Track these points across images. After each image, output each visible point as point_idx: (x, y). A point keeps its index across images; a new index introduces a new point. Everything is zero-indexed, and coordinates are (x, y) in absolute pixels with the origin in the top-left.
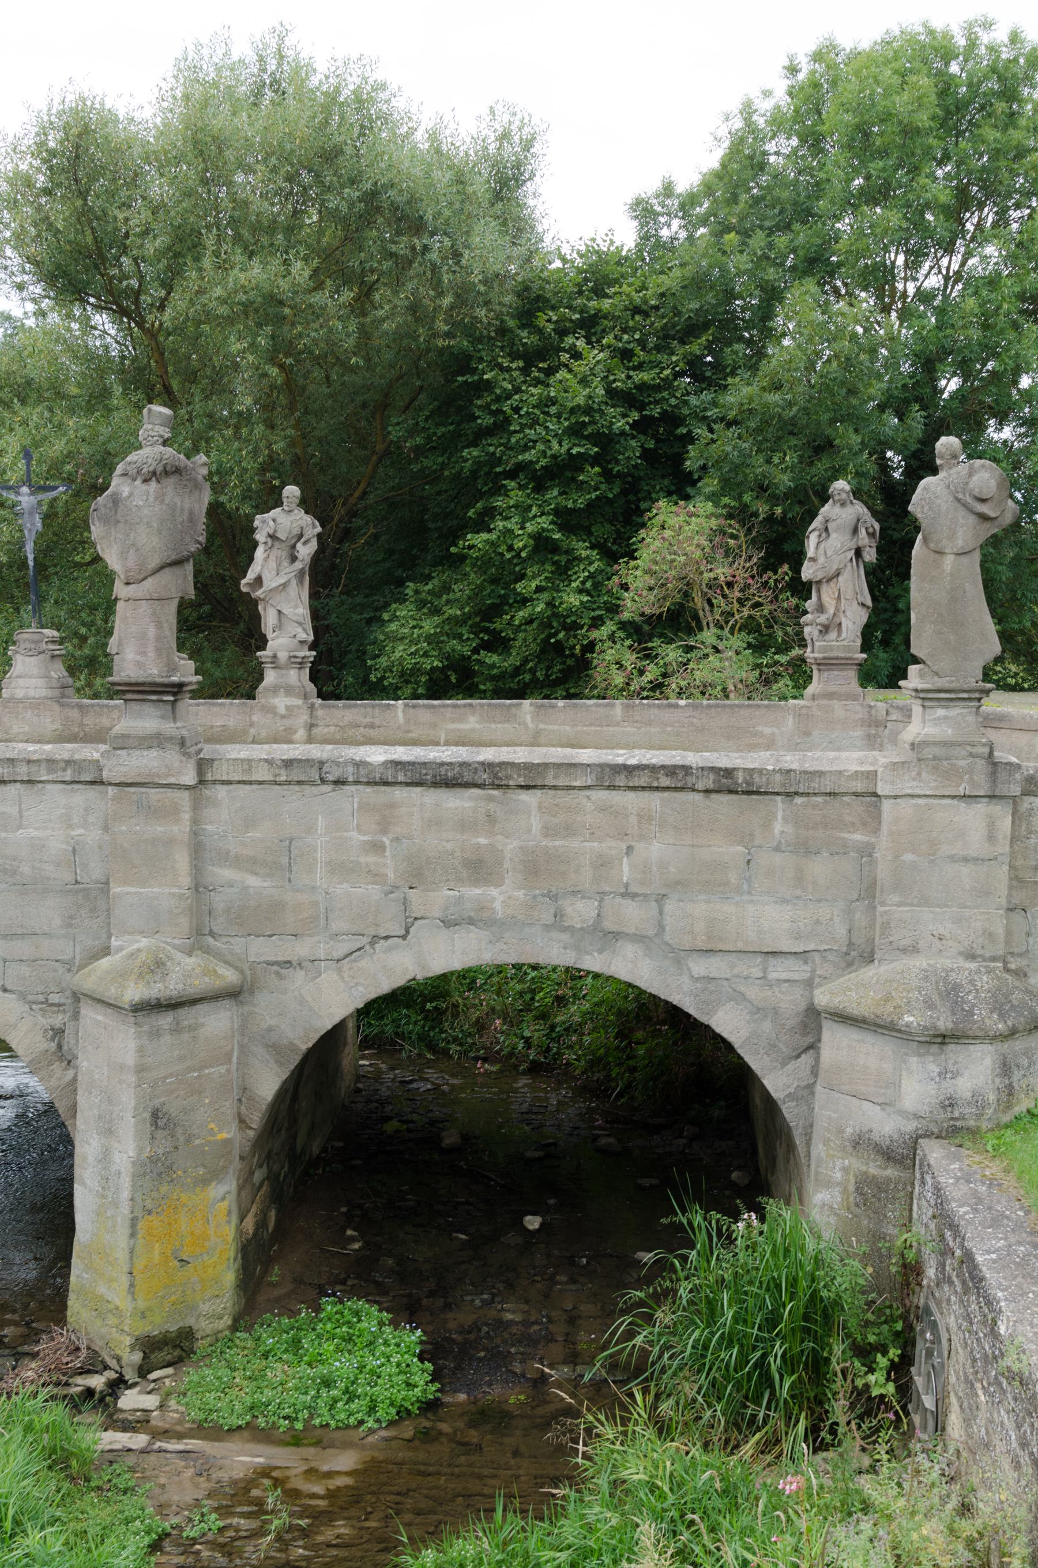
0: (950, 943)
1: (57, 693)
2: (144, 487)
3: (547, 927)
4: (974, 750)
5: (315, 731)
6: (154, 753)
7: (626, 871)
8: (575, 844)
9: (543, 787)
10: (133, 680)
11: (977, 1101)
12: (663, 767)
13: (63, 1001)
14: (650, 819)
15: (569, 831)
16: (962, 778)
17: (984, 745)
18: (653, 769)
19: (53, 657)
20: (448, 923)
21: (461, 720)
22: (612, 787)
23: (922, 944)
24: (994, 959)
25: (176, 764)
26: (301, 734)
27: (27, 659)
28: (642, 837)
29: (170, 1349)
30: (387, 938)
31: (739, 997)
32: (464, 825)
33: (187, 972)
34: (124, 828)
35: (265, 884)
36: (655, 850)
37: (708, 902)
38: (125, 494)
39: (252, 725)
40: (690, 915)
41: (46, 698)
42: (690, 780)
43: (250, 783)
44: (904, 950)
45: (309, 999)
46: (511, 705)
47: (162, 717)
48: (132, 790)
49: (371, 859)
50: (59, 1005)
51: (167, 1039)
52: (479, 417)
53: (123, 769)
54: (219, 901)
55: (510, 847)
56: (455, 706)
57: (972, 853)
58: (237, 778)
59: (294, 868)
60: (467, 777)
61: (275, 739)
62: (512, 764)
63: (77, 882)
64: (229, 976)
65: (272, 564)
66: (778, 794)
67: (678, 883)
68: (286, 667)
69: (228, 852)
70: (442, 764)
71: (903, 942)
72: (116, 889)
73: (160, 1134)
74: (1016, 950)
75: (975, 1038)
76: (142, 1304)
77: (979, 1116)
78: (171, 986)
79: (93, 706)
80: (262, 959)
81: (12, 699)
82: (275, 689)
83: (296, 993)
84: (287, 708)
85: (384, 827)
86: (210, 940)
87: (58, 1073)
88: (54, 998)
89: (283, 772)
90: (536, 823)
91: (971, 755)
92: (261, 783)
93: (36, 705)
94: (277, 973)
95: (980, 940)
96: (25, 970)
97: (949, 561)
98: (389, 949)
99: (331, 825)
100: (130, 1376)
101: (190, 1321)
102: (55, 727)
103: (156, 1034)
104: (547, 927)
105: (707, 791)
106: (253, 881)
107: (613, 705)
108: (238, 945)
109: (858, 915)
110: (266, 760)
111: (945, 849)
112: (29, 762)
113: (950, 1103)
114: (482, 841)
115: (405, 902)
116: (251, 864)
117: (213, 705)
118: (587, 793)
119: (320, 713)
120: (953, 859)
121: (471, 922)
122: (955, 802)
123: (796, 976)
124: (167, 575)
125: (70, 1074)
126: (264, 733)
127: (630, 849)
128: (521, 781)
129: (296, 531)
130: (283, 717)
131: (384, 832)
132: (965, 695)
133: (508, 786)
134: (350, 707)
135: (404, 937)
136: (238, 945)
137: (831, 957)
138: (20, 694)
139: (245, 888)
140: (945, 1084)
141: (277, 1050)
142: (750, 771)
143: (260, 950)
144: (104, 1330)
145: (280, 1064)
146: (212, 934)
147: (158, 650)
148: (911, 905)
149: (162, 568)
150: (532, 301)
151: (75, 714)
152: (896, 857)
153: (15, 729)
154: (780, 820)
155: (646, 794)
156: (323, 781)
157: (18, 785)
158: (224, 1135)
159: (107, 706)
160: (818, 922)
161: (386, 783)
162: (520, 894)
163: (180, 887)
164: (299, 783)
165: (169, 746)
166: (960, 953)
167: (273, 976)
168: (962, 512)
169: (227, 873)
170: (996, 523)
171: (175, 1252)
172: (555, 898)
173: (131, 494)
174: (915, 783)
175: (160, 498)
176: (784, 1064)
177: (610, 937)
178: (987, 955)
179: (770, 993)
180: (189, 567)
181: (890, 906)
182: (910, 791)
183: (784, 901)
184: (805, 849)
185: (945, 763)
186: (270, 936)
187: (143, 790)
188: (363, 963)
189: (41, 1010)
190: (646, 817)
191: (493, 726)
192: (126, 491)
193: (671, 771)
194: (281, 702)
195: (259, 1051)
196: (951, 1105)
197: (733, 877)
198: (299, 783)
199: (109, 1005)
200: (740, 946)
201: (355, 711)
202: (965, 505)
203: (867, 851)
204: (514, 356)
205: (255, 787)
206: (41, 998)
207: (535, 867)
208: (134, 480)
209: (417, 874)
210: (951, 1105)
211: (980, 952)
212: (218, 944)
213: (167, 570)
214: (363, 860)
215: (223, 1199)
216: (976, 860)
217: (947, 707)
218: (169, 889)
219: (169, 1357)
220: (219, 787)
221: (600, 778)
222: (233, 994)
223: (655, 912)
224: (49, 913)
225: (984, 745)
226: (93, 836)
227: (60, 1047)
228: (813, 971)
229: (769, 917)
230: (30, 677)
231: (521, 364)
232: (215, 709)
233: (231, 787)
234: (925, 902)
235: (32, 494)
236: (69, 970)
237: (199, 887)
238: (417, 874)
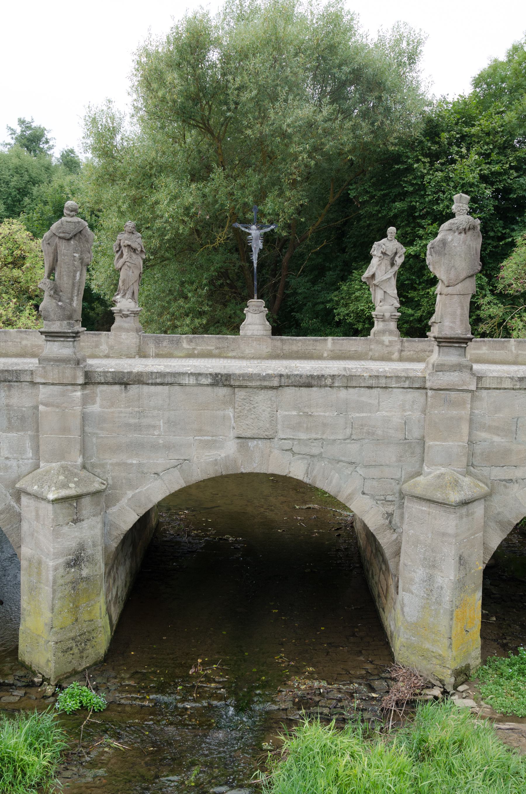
2: (459, 236)
5: (403, 353)
6: (456, 374)
10: (449, 336)
13: (393, 499)
21: (479, 348)
25: (468, 380)
26: (396, 355)
27: (254, 315)
34: (436, 412)
35: (503, 440)
38: (449, 240)
39: (371, 350)
41: (263, 335)
43: (500, 389)
45: (520, 498)
46: (504, 341)
47: (460, 355)
48: (442, 392)
50: (392, 501)
52: (405, 187)
53: (440, 382)
54: (478, 449)
58: (494, 387)
59: (518, 432)
61: (383, 359)
63: (405, 439)
65: (383, 267)
68: (388, 321)
69: (485, 424)
72: (429, 443)
79: (288, 340)
80: (498, 478)
81: (245, 336)
82: (121, 328)
83: (513, 495)
84: (390, 342)
86: (472, 468)
87: (388, 536)
88: (389, 498)
89: (518, 383)
92: (505, 389)
93: (258, 339)
94: (505, 485)
96: (375, 483)
102: (268, 350)
108: (486, 471)
110: (510, 378)
112: (386, 377)
116: (495, 430)
117: (351, 339)
119: (406, 344)
125: (395, 536)
126: (377, 355)
129: (394, 251)
130: (387, 346)
134: (422, 341)
136: (486, 471)
138: (249, 333)
139: (493, 442)
141: (501, 524)
143: (497, 473)
144: (429, 666)
145: (503, 531)
149: (464, 280)
150: (433, 129)
151: (279, 344)
153: (247, 351)
157: (379, 389)
159: (296, 340)
163: (463, 442)
165: (465, 370)
167: (502, 487)
169: (483, 435)
173: (452, 240)
180: (475, 278)
186: (503, 467)
187: (448, 392)
189: (382, 503)
191: (495, 352)
192: (450, 238)
194: (386, 339)
195: (492, 524)
199: (441, 503)
201: (424, 343)
204: (426, 156)
205: (502, 391)
206: (382, 498)
208: (455, 232)
212: (476, 471)
213: (468, 279)
218: (456, 444)
219: (462, 679)
220: (483, 391)
222: (486, 497)
224: (390, 455)
226: (416, 415)
227: (390, 522)
230: (255, 324)
231: (429, 160)
232: (351, 342)
233: (489, 391)
235: (258, 229)
236: (398, 484)
237: (471, 442)
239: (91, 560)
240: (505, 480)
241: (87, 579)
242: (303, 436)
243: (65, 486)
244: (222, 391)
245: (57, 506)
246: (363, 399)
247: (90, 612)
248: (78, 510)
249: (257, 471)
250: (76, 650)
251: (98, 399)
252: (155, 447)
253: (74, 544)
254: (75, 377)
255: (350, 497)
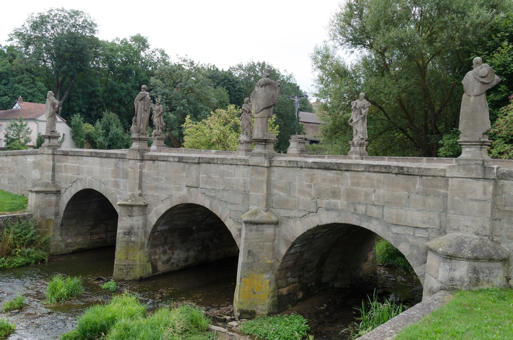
0: (470, 229)
1: (299, 152)
3: (352, 213)
4: (477, 162)
6: (259, 158)
7: (373, 198)
8: (360, 188)
9: (351, 171)
11: (461, 280)
12: (383, 166)
14: (380, 182)
15: (358, 184)
16: (473, 172)
17: (480, 160)
18: (380, 166)
19: (299, 143)
20: (327, 210)
22: (369, 171)
23: (461, 228)
24: (485, 236)
28: (378, 187)
29: (249, 315)
30: (312, 212)
31: (407, 241)
32: (331, 181)
33: (263, 216)
36: (381, 191)
37: (396, 209)
40: (391, 213)
42: (391, 170)
43: (281, 167)
44: (455, 230)
49: (308, 189)
51: (254, 232)
54: (274, 198)
55: (343, 188)
56: (403, 159)
57: (478, 198)
60: (332, 167)
62: (343, 164)
64: (274, 219)
66: (417, 175)
67: (388, 202)
68: (356, 146)
70: (325, 163)
71: (454, 227)
73: (250, 257)
74: (497, 234)
75: (461, 258)
76: (241, 301)
77: (462, 286)
78: (257, 219)
82: (352, 152)
85: (312, 180)
90: (349, 183)
91: (476, 164)
92: (284, 167)
95: (481, 229)
96: (234, 213)
97: (472, 98)
98: (312, 216)
99: (300, 179)
100: (237, 319)
101: (255, 309)
103: (251, 230)
104: (352, 213)
105: (396, 174)
106: (282, 194)
107: (452, 160)
109: (443, 217)
111: (469, 196)
112: (236, 159)
113: (452, 280)
114: (336, 186)
115: (316, 203)
116: (281, 189)
118: (363, 173)
120: (471, 200)
121: (333, 210)
122: (472, 180)
123: (424, 236)
124: (265, 111)
127: (374, 190)
128: (345, 169)
131: (312, 182)
132: (475, 143)
133: (342, 170)
135: (316, 213)
137: (435, 230)
138: (291, 152)
140: (451, 273)
141: (286, 241)
142: (408, 168)
143: (283, 213)
146: (273, 207)
147: (261, 131)
148: (458, 214)
149: (263, 109)
152: (452, 198)
154: (418, 184)
155: (379, 174)
156: (298, 167)
158: (269, 262)
160: (430, 218)
161: (312, 168)
162: (345, 202)
164: (292, 167)
166: (474, 233)
168: (476, 82)
170: (490, 85)
171: (252, 289)
172: (354, 204)
174: (458, 173)
175: (265, 91)
176: (420, 265)
177: (370, 218)
178: (483, 234)
179: (416, 241)
181: (451, 215)
182: (456, 176)
183: (420, 211)
184: (426, 194)
185: (467, 166)
188: (307, 219)
190: (379, 181)
193: (385, 167)
196: (452, 280)
197: (404, 202)
198: (292, 167)
200: (406, 224)
202: (477, 79)
203: (445, 196)
207: (349, 194)
209: (319, 195)
210: (452, 280)
211: (480, 233)
214: (306, 189)
215: (268, 279)
216: (479, 201)
217: (470, 148)
218: (262, 194)
221: (366, 168)
222: (276, 224)
223: (382, 211)
224: (239, 199)
225: (480, 160)
228: (429, 235)
229: (414, 216)
234: (462, 214)
238: (319, 195)
239: (136, 234)
240: (286, 217)
241: (134, 242)
242: (208, 187)
243: (127, 200)
244: (182, 164)
245: (121, 208)
246: (229, 170)
247: (134, 257)
248: (131, 211)
249: (193, 203)
250: (125, 271)
251: (146, 167)
252: (162, 189)
253: (128, 226)
254: (137, 157)
255: (225, 219)
